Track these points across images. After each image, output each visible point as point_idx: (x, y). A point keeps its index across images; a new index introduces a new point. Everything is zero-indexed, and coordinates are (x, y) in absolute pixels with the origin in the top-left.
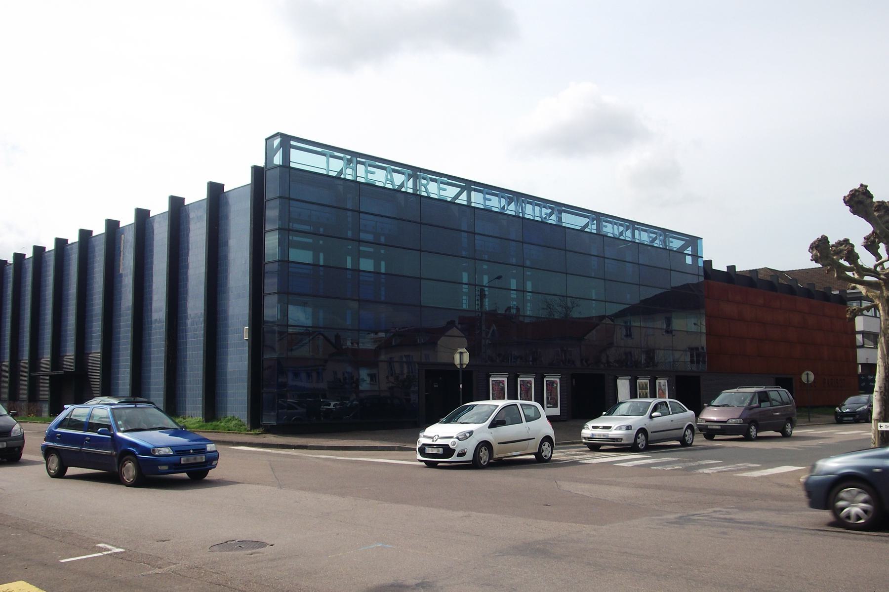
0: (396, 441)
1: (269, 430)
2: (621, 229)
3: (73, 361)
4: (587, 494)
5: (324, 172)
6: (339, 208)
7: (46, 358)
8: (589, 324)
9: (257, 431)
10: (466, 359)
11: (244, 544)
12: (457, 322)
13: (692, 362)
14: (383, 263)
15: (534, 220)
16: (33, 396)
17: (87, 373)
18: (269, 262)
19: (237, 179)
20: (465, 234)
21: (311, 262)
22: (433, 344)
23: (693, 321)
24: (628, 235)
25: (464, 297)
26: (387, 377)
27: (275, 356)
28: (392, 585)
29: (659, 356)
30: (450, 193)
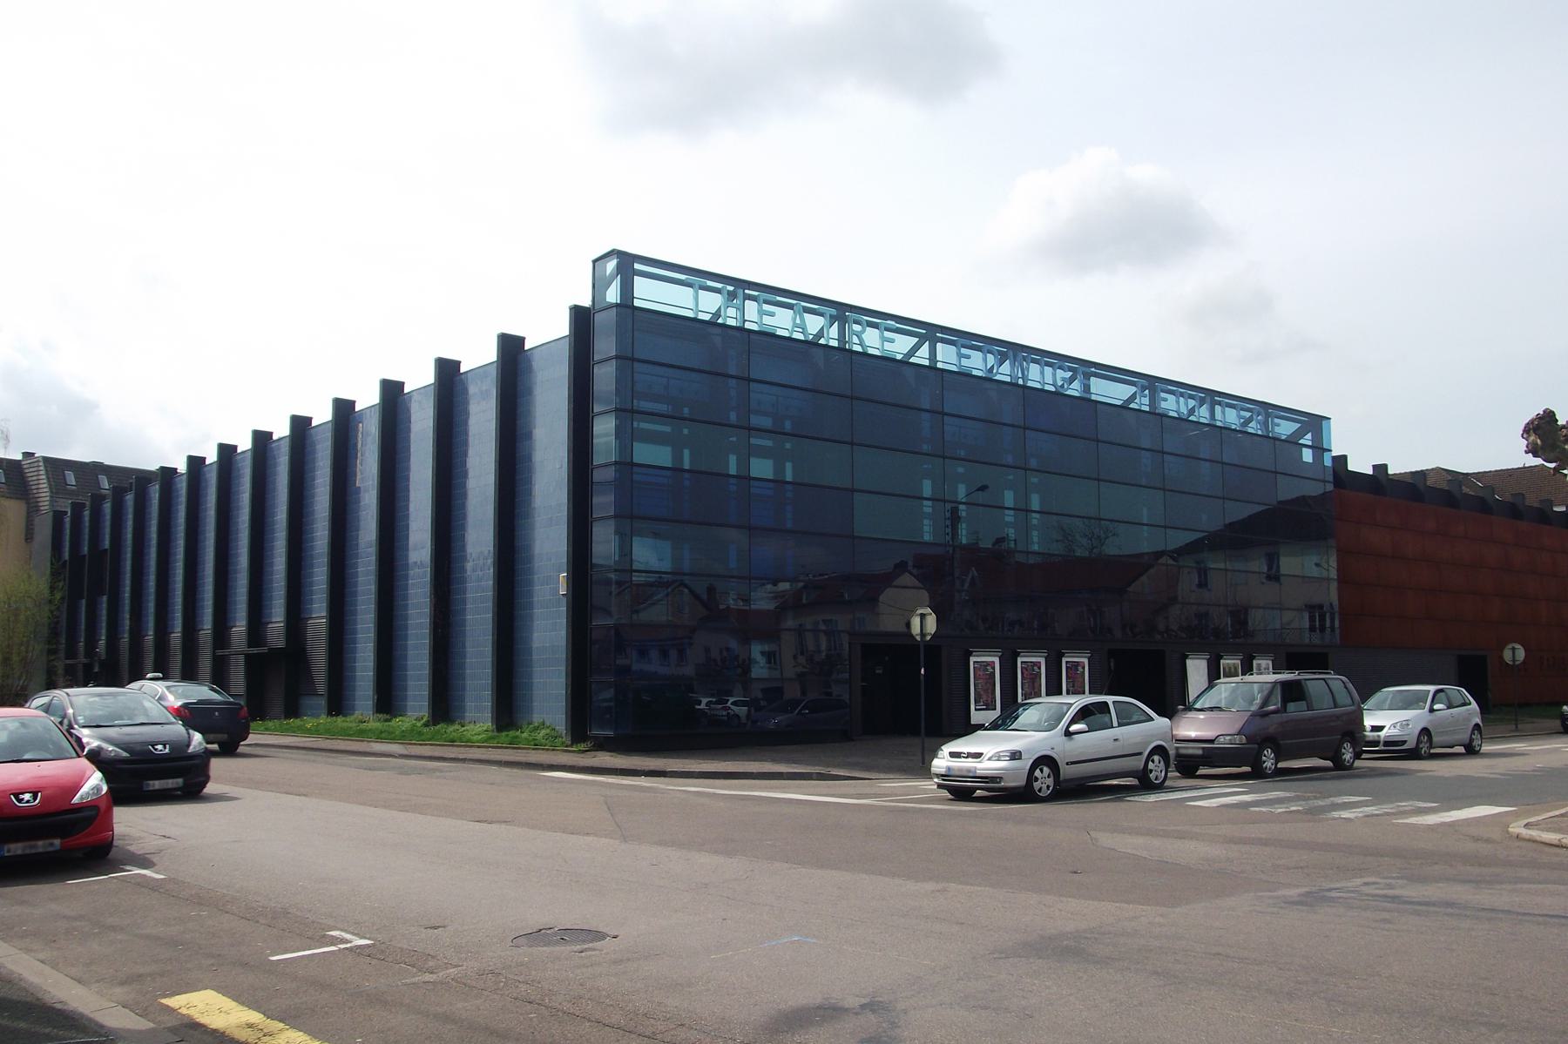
0: (808, 764)
1: (602, 745)
2: (1192, 403)
3: (283, 631)
4: (1145, 854)
5: (690, 314)
6: (718, 374)
7: (240, 626)
8: (1135, 566)
9: (582, 747)
10: (931, 625)
11: (568, 935)
12: (910, 563)
13: (1312, 629)
14: (789, 466)
15: (1043, 390)
17: (304, 650)
19: (546, 328)
20: (925, 416)
21: (771, 477)
22: (872, 601)
23: (1315, 559)
24: (1203, 414)
25: (926, 522)
26: (795, 657)
27: (610, 622)
28: (819, 1007)
29: (1256, 619)
30: (900, 346)
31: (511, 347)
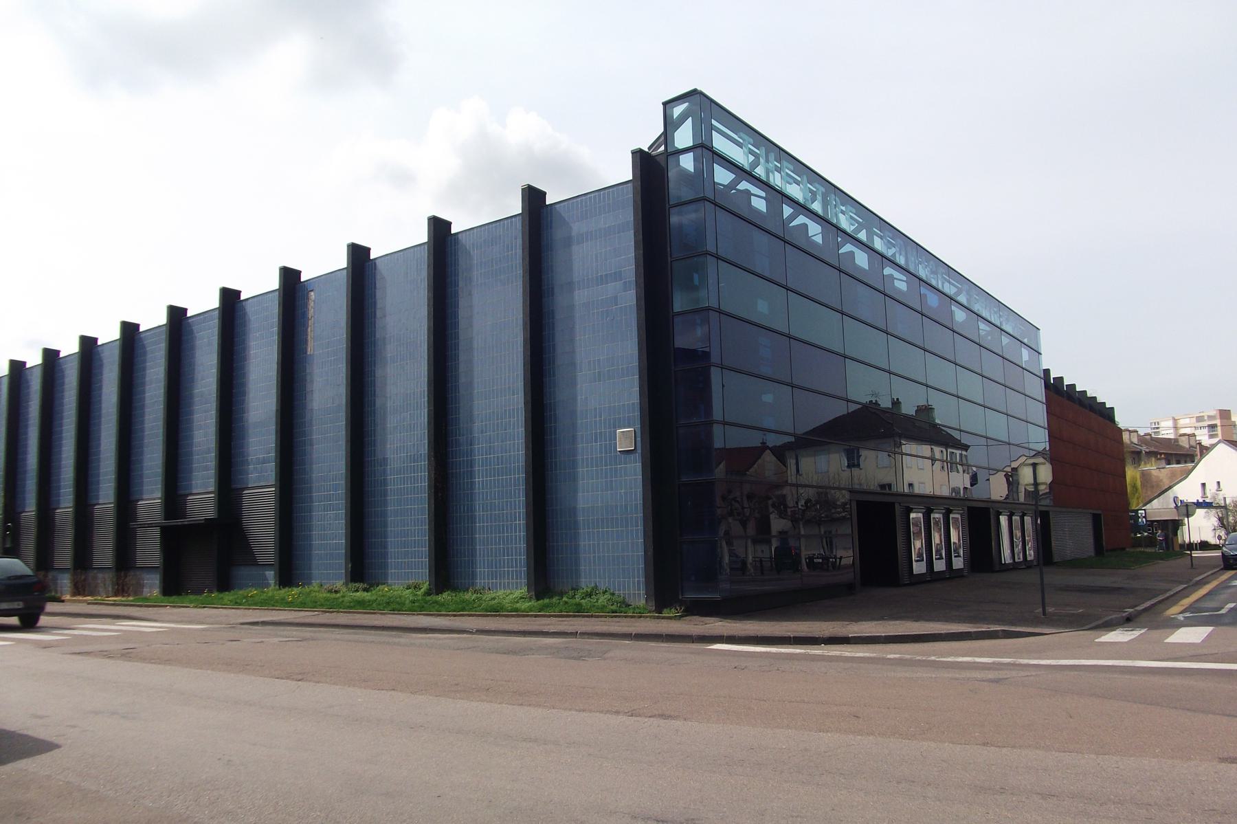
7: (151, 497)
16: (125, 561)
18: (679, 314)
31: (230, 297)
